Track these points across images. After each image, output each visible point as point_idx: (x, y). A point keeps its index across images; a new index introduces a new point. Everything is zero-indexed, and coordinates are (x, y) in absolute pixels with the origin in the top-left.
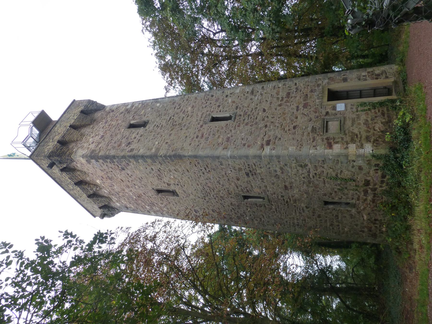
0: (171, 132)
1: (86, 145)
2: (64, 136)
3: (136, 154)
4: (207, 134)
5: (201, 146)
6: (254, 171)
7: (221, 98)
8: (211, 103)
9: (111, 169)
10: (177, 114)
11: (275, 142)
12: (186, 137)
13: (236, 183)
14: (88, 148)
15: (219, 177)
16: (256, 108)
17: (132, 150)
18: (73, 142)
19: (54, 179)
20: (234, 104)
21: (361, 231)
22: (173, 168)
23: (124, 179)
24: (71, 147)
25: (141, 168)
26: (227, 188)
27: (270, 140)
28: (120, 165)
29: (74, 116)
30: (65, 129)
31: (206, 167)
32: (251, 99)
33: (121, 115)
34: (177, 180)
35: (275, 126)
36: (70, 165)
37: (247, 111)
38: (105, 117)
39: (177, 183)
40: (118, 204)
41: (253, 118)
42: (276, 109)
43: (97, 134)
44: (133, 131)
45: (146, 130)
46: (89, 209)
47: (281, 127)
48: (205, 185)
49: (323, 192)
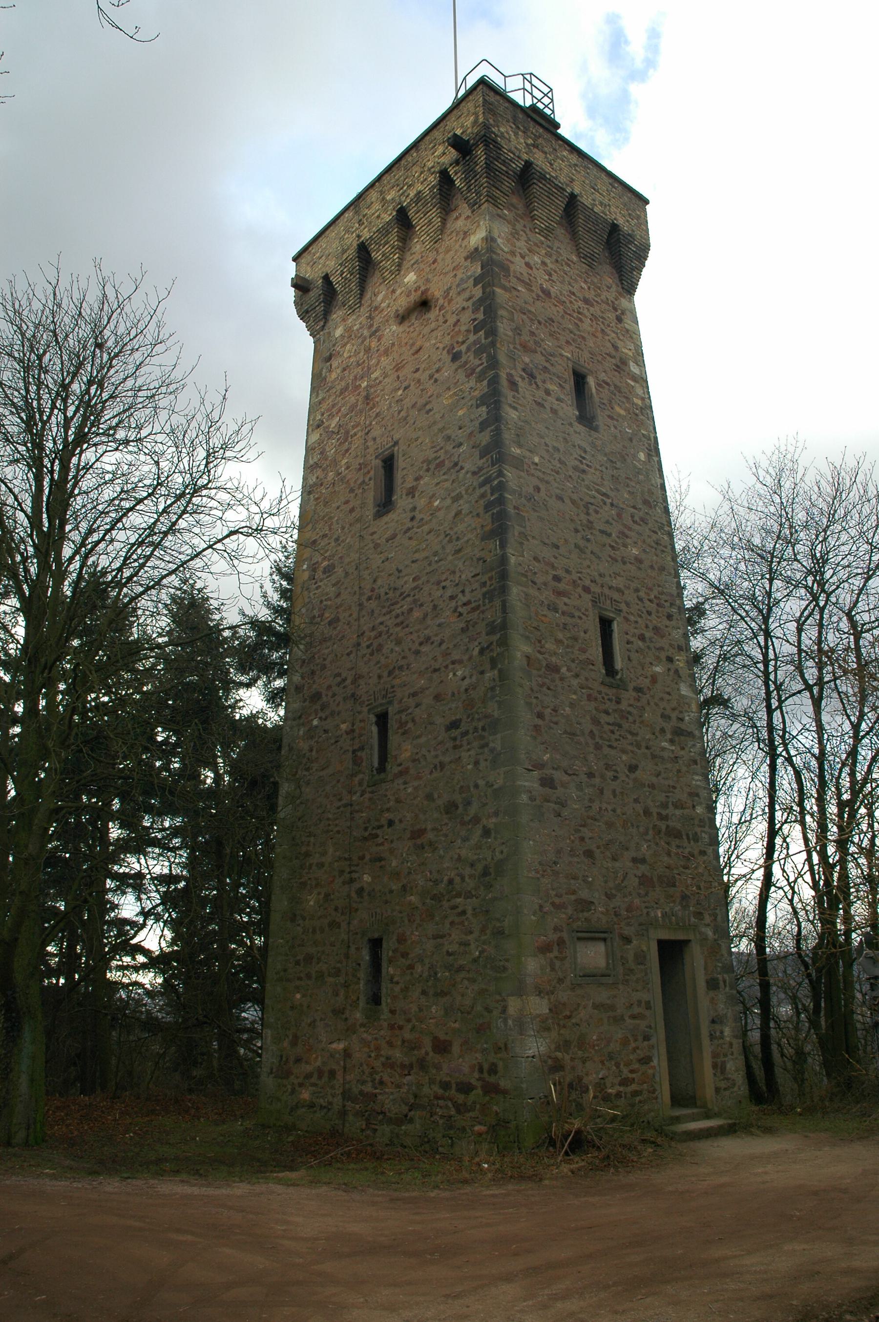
0: (567, 501)
1: (521, 244)
2: (545, 178)
3: (503, 399)
4: (565, 608)
5: (532, 592)
6: (465, 743)
7: (663, 643)
8: (649, 613)
9: (452, 320)
10: (619, 515)
11: (548, 801)
12: (557, 547)
13: (427, 692)
14: (513, 253)
15: (442, 643)
16: (639, 746)
17: (513, 385)
18: (529, 206)
19: (415, 145)
20: (647, 681)
21: (296, 1037)
22: (466, 508)
23: (423, 356)
24: (515, 200)
25: (460, 413)
26: (408, 665)
27: (556, 789)
28: (468, 349)
29: (601, 204)
30: (563, 179)
31: (473, 605)
32: (663, 730)
33: (609, 345)
34: (427, 518)
35: (591, 800)
36: (459, 196)
37: (631, 719)
38: (603, 297)
39: (419, 517)
40: (338, 332)
41: (613, 737)
42: (636, 801)
43: (555, 278)
44: (567, 386)
45: (571, 424)
46: (323, 242)
47: (588, 817)
48: (415, 601)
49: (408, 933)
